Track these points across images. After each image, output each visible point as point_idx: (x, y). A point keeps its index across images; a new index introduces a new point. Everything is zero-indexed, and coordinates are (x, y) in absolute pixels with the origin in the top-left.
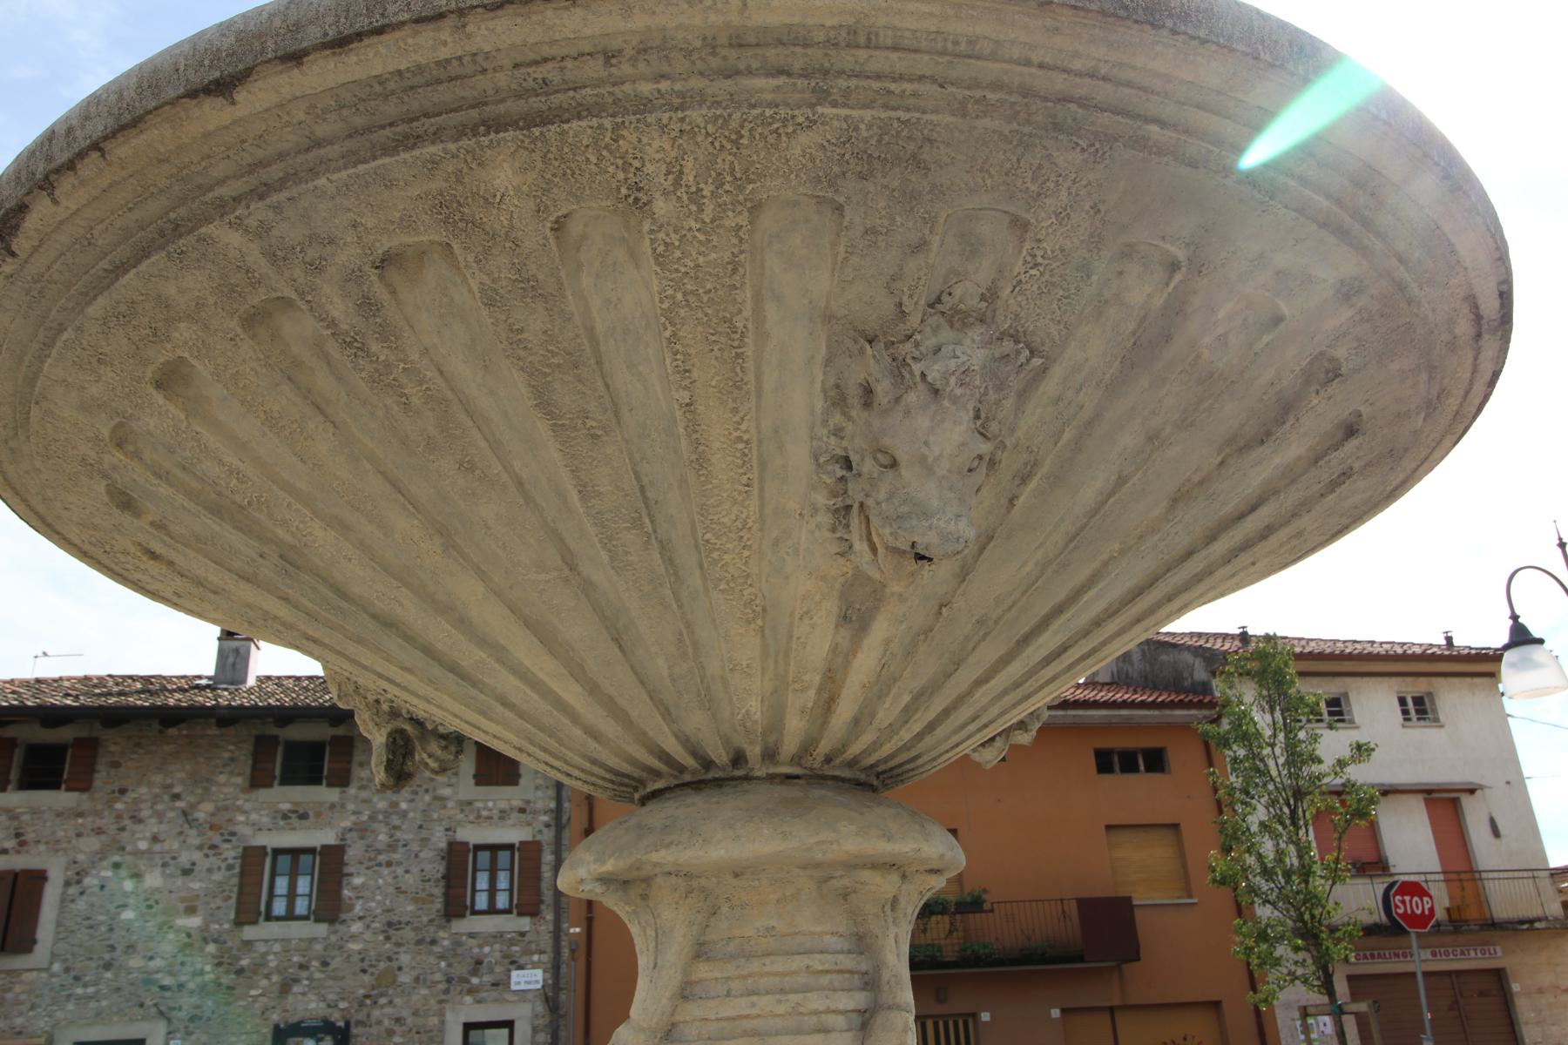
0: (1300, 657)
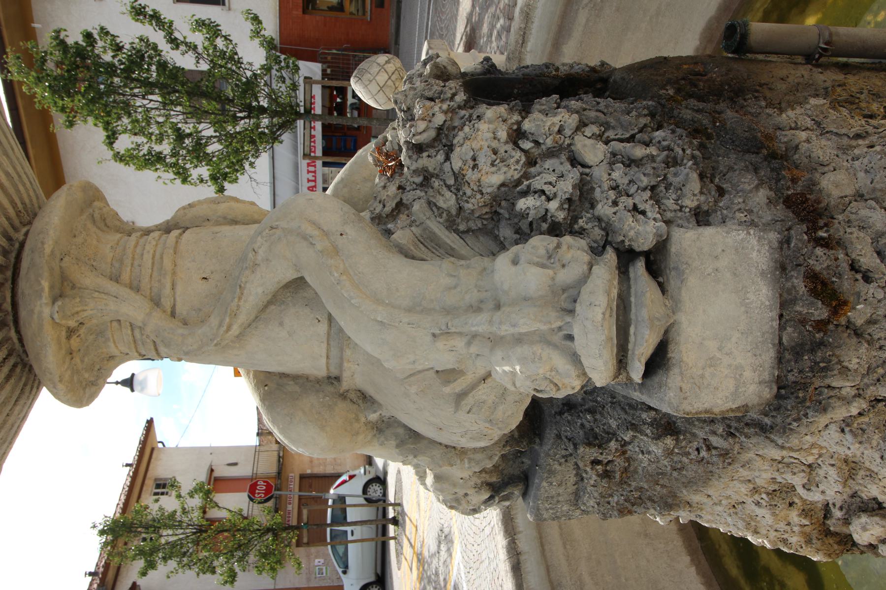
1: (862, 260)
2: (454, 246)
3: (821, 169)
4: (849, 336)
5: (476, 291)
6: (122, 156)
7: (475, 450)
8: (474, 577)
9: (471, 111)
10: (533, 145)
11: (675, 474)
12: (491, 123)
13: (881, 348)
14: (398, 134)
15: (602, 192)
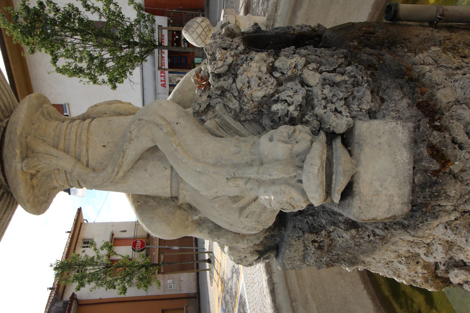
0: (67, 257)
1: (458, 138)
2: (238, 129)
3: (437, 87)
4: (450, 179)
5: (250, 155)
6: (61, 70)
7: (250, 235)
8: (251, 291)
9: (247, 55)
10: (281, 74)
11: (356, 248)
12: (258, 63)
13: (467, 184)
14: (207, 67)
15: (318, 101)
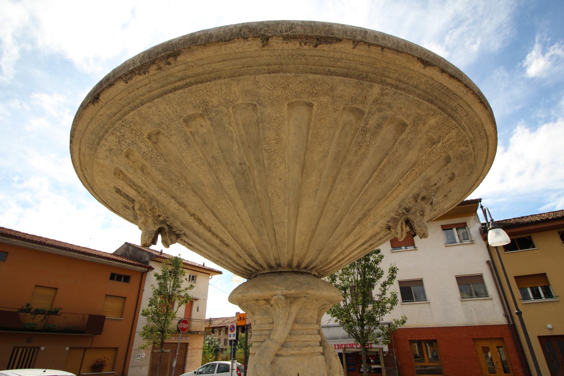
0: (184, 263)
